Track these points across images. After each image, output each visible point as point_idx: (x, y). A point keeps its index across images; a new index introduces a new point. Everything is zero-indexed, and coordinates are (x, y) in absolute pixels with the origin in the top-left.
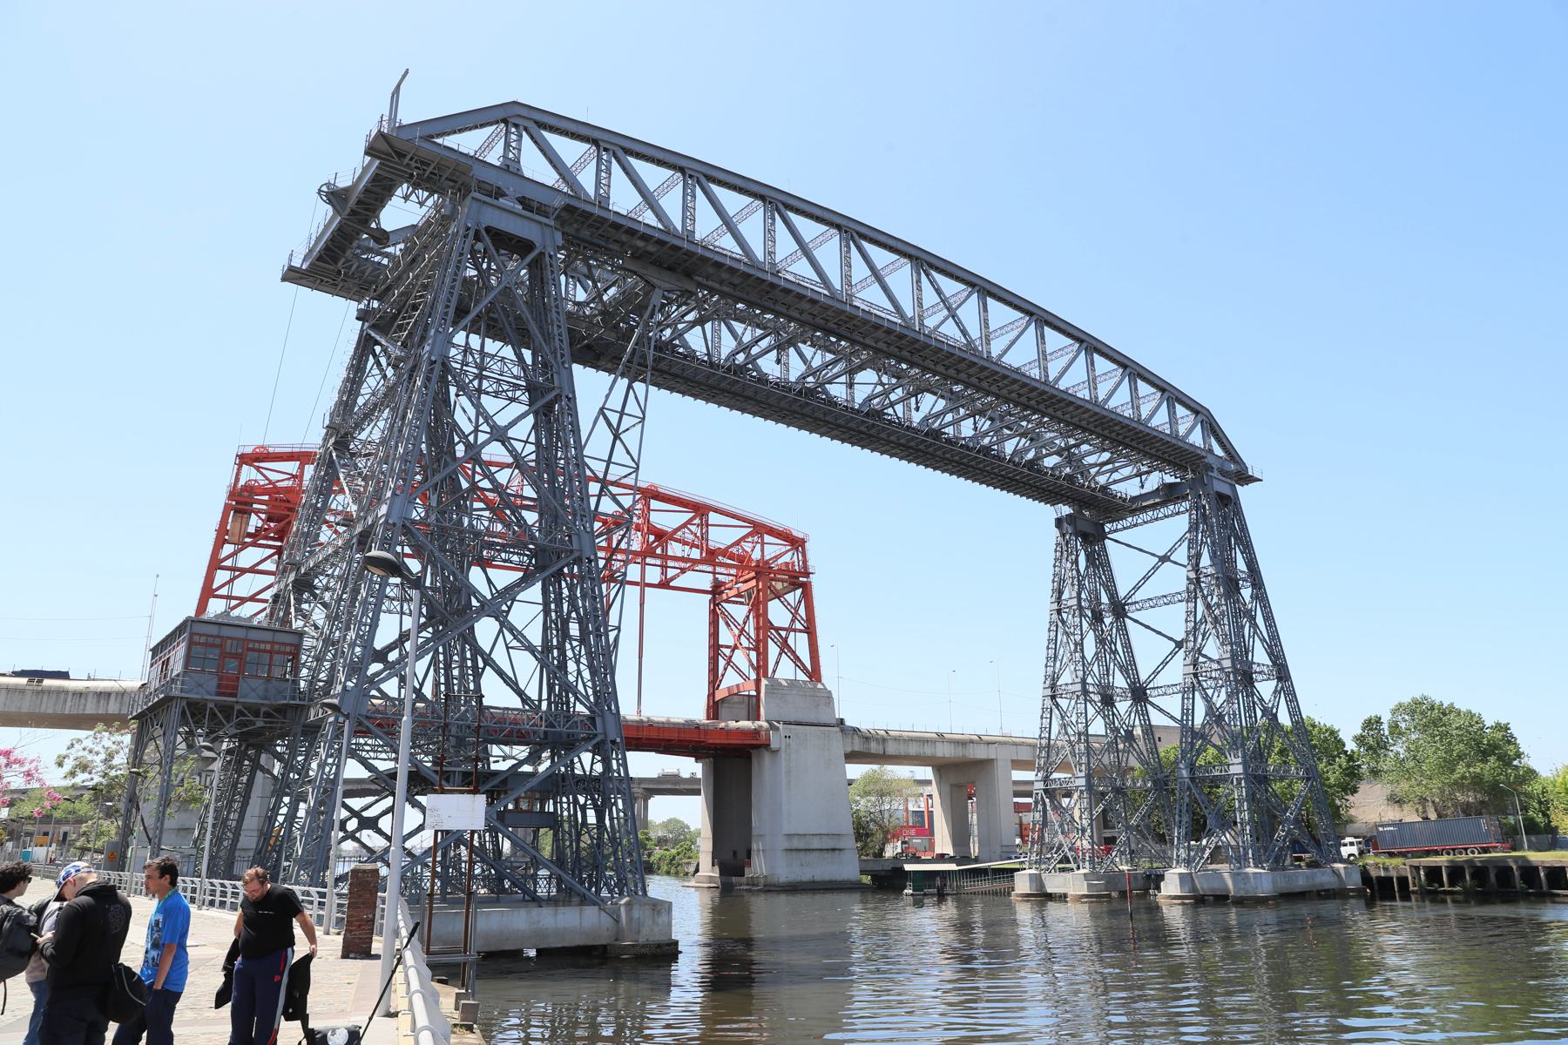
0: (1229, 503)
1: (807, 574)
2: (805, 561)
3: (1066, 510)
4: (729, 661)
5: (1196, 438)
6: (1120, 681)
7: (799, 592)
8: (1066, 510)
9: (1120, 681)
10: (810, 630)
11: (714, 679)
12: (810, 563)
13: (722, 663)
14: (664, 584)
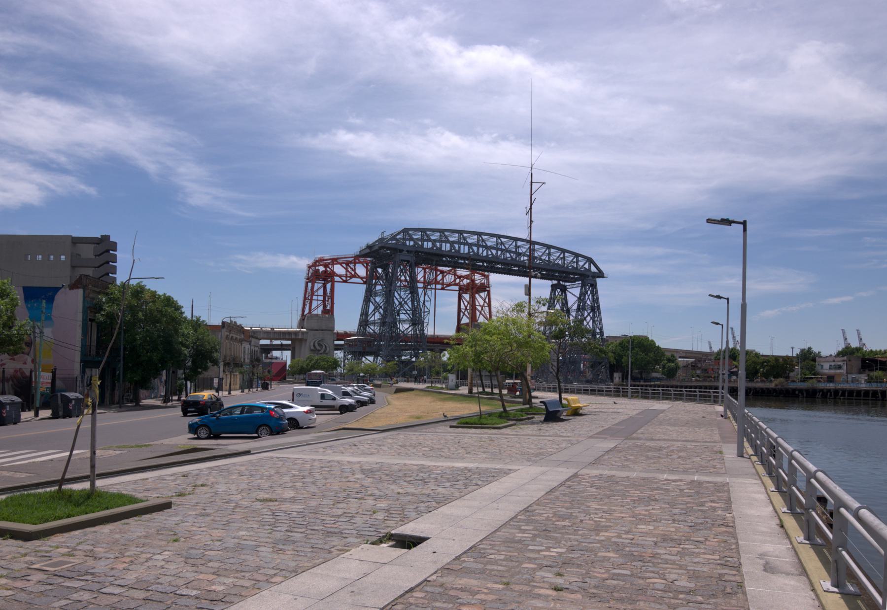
0: (594, 286)
1: (489, 287)
2: (488, 282)
3: (555, 282)
4: (464, 314)
5: (587, 266)
6: (598, 331)
7: (486, 292)
8: (555, 282)
9: (598, 331)
10: (489, 306)
11: (459, 320)
12: (490, 283)
13: (462, 314)
14: (443, 289)
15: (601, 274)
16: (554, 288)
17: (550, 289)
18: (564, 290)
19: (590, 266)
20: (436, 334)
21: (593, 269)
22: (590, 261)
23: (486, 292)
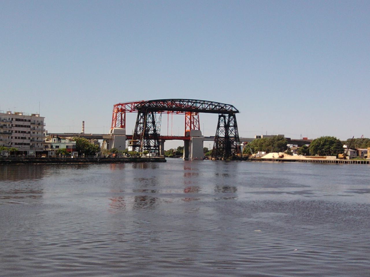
0: (235, 117)
3: (221, 114)
7: (197, 116)
8: (221, 114)
15: (238, 112)
16: (220, 117)
17: (218, 117)
18: (225, 117)
19: (232, 108)
20: (169, 135)
21: (234, 110)
22: (232, 106)
23: (197, 116)
